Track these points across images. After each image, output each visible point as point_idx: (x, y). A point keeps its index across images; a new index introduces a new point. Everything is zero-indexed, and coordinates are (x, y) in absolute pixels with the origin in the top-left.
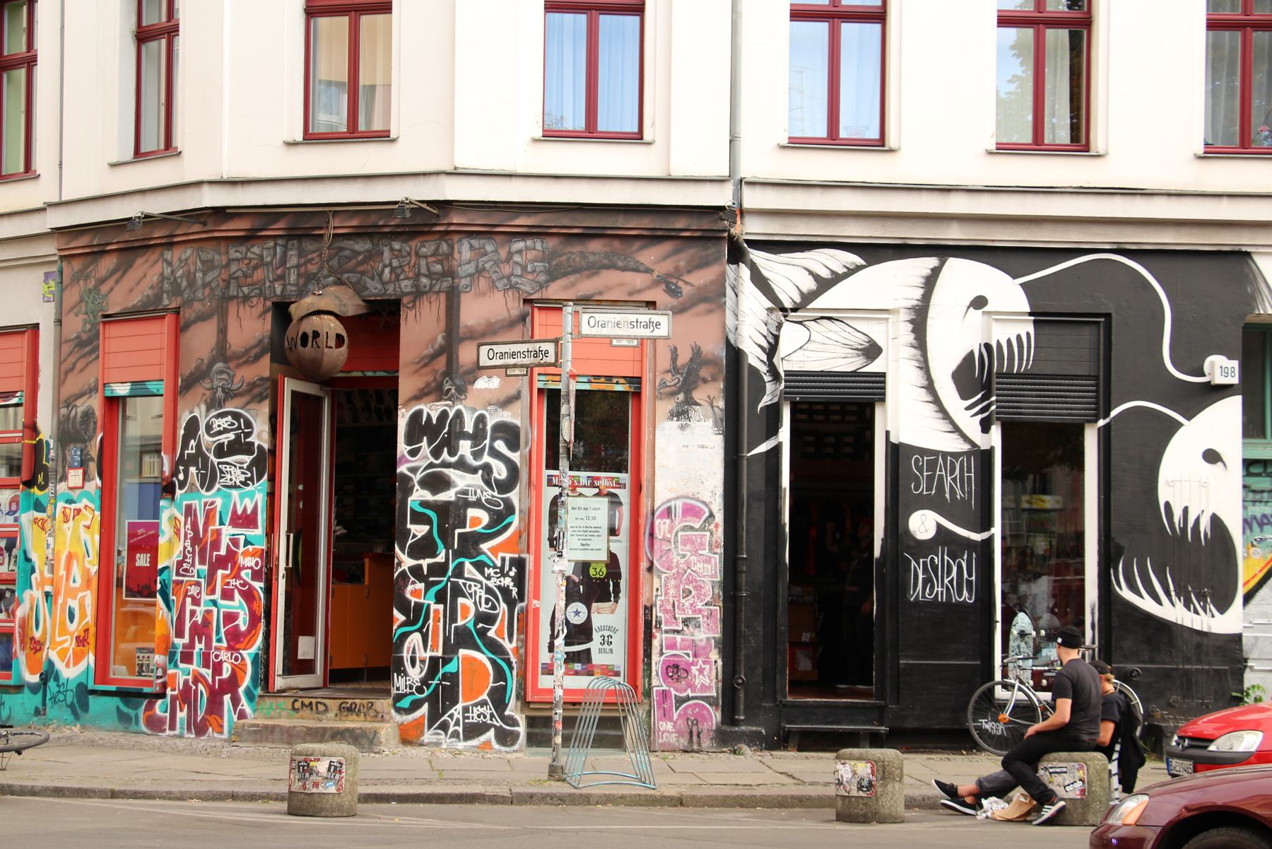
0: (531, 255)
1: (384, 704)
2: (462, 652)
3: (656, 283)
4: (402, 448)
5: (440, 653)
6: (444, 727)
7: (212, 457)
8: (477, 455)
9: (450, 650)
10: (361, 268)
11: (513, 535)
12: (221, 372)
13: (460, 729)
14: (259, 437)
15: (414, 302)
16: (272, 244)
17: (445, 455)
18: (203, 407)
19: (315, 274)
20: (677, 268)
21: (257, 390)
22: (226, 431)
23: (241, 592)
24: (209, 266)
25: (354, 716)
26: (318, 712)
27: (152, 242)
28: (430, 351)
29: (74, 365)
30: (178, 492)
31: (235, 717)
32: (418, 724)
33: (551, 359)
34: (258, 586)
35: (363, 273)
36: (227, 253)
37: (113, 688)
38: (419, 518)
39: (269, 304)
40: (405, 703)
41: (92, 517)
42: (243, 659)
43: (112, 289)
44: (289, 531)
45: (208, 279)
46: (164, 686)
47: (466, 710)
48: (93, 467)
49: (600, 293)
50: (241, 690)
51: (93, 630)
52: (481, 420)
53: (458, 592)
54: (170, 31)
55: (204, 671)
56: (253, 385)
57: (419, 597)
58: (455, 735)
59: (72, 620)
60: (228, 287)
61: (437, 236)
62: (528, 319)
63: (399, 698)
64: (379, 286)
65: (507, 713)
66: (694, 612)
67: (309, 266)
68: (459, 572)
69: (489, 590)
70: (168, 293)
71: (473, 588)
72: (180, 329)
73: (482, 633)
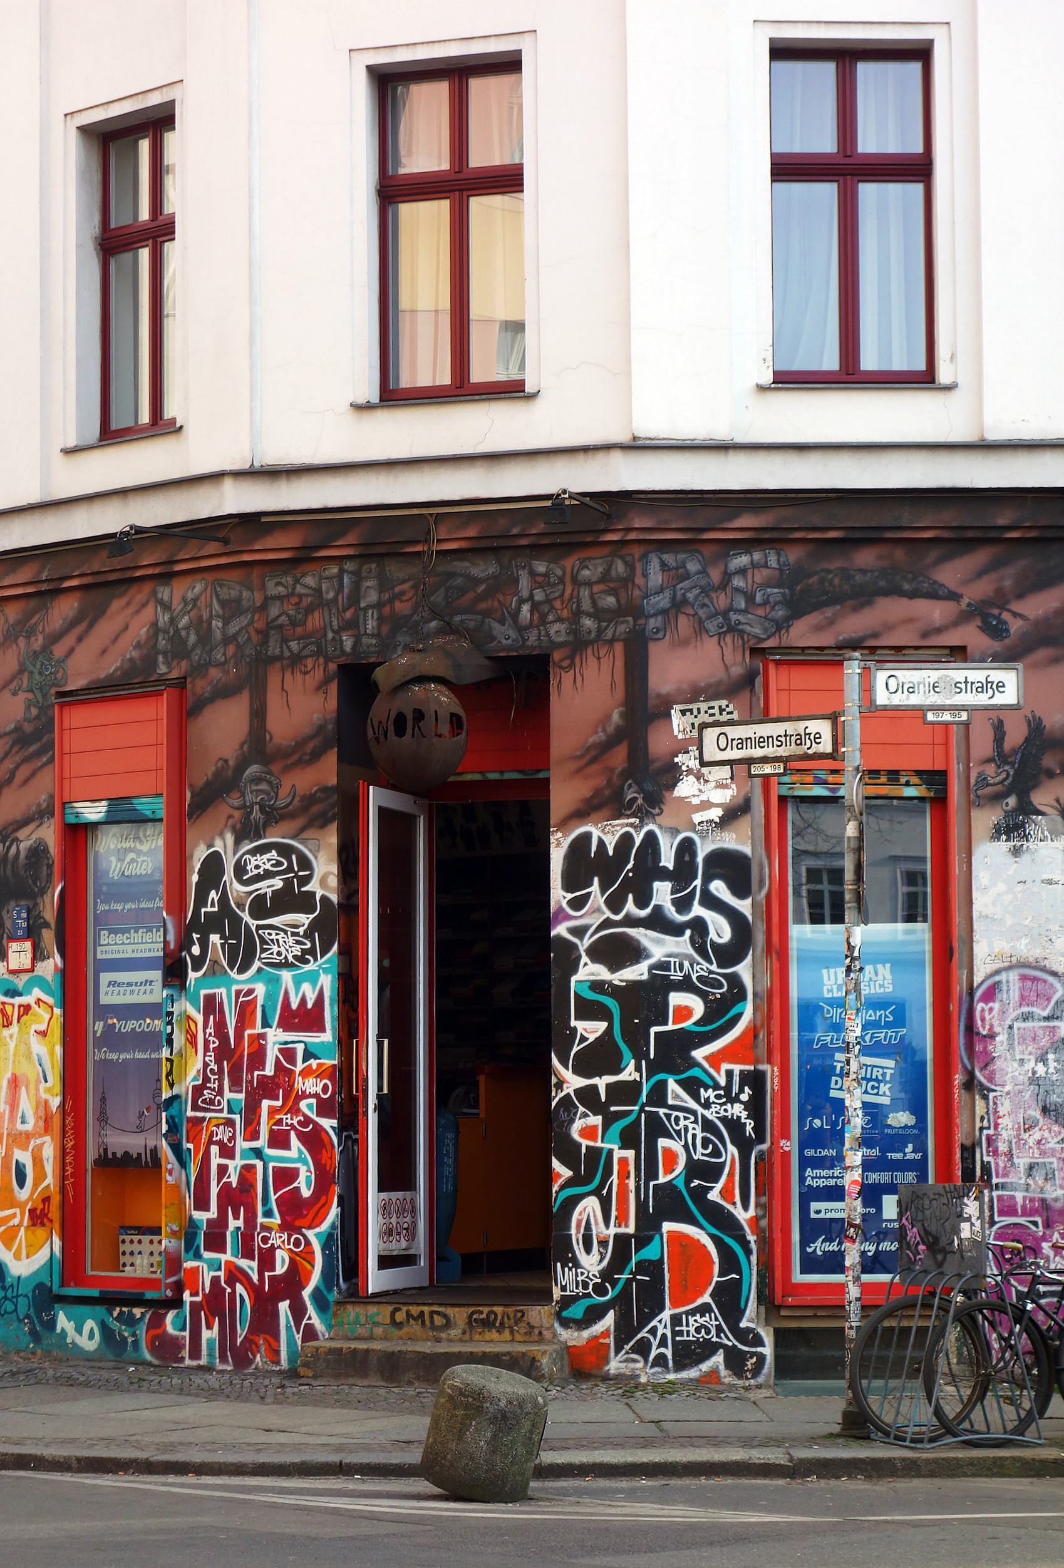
0: (760, 576)
1: (539, 1314)
2: (667, 1226)
3: (964, 617)
4: (559, 896)
5: (631, 1229)
6: (643, 1349)
7: (246, 917)
8: (683, 905)
9: (648, 1225)
10: (483, 605)
11: (744, 1033)
12: (257, 780)
13: (669, 1353)
14: (323, 883)
15: (572, 658)
16: (335, 570)
17: (630, 906)
18: (230, 838)
19: (408, 617)
20: (999, 591)
21: (316, 809)
22: (268, 875)
23: (301, 1136)
24: (232, 609)
25: (494, 1335)
26: (433, 1327)
27: (138, 574)
28: (601, 736)
29: (13, 774)
30: (192, 975)
31: (298, 1337)
32: (597, 1349)
33: (826, 746)
34: (328, 1124)
35: (487, 614)
36: (263, 587)
37: (95, 1293)
38: (589, 1010)
39: (333, 667)
40: (576, 1311)
41: (47, 1016)
42: (308, 1243)
43: (71, 651)
44: (381, 1035)
45: (232, 629)
46: (179, 1288)
47: (676, 1320)
48: (48, 937)
49: (875, 635)
50: (306, 1293)
51: (56, 1200)
52: (686, 848)
53: (658, 1129)
54: (161, 230)
55: (244, 1263)
56: (309, 800)
57: (595, 1139)
58: (661, 1360)
59: (21, 1183)
60: (265, 642)
61: (606, 550)
62: (759, 681)
63: (567, 1301)
64: (513, 634)
65: (743, 1324)
66: (1043, 1153)
67: (398, 605)
68: (659, 1095)
69: (708, 1125)
70: (165, 654)
71: (682, 1123)
72: (186, 712)
73: (700, 1195)
